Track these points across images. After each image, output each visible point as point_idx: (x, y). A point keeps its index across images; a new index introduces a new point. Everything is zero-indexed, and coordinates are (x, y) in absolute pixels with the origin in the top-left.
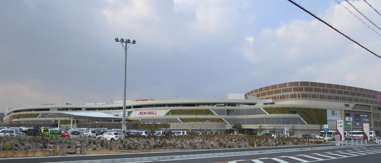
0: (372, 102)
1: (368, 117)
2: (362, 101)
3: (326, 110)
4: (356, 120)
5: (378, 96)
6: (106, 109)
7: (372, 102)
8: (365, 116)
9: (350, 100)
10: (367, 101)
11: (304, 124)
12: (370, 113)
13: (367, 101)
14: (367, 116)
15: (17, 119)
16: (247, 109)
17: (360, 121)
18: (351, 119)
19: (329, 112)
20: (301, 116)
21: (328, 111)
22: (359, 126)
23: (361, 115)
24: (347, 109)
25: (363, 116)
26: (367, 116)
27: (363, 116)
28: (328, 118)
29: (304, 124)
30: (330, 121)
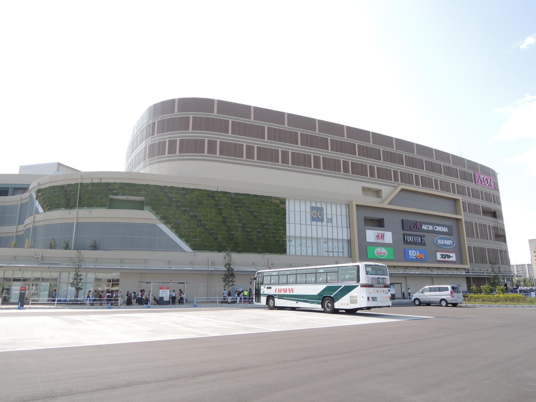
0: (461, 190)
1: (449, 234)
2: (427, 182)
3: (283, 202)
4: (405, 242)
5: (481, 176)
6: (367, 286)
7: (461, 190)
8: (439, 229)
9: (384, 175)
10: (445, 186)
11: (176, 248)
12: (458, 220)
13: (445, 186)
14: (445, 230)
15: (439, 292)
16: (78, 224)
17: (422, 243)
18: (388, 237)
19: (298, 214)
20: (166, 220)
21: (291, 207)
22: (417, 260)
23: (424, 227)
24: (371, 201)
25: (431, 228)
26: (445, 230)
27: (431, 228)
28: (291, 230)
29: (176, 248)
30: (304, 241)
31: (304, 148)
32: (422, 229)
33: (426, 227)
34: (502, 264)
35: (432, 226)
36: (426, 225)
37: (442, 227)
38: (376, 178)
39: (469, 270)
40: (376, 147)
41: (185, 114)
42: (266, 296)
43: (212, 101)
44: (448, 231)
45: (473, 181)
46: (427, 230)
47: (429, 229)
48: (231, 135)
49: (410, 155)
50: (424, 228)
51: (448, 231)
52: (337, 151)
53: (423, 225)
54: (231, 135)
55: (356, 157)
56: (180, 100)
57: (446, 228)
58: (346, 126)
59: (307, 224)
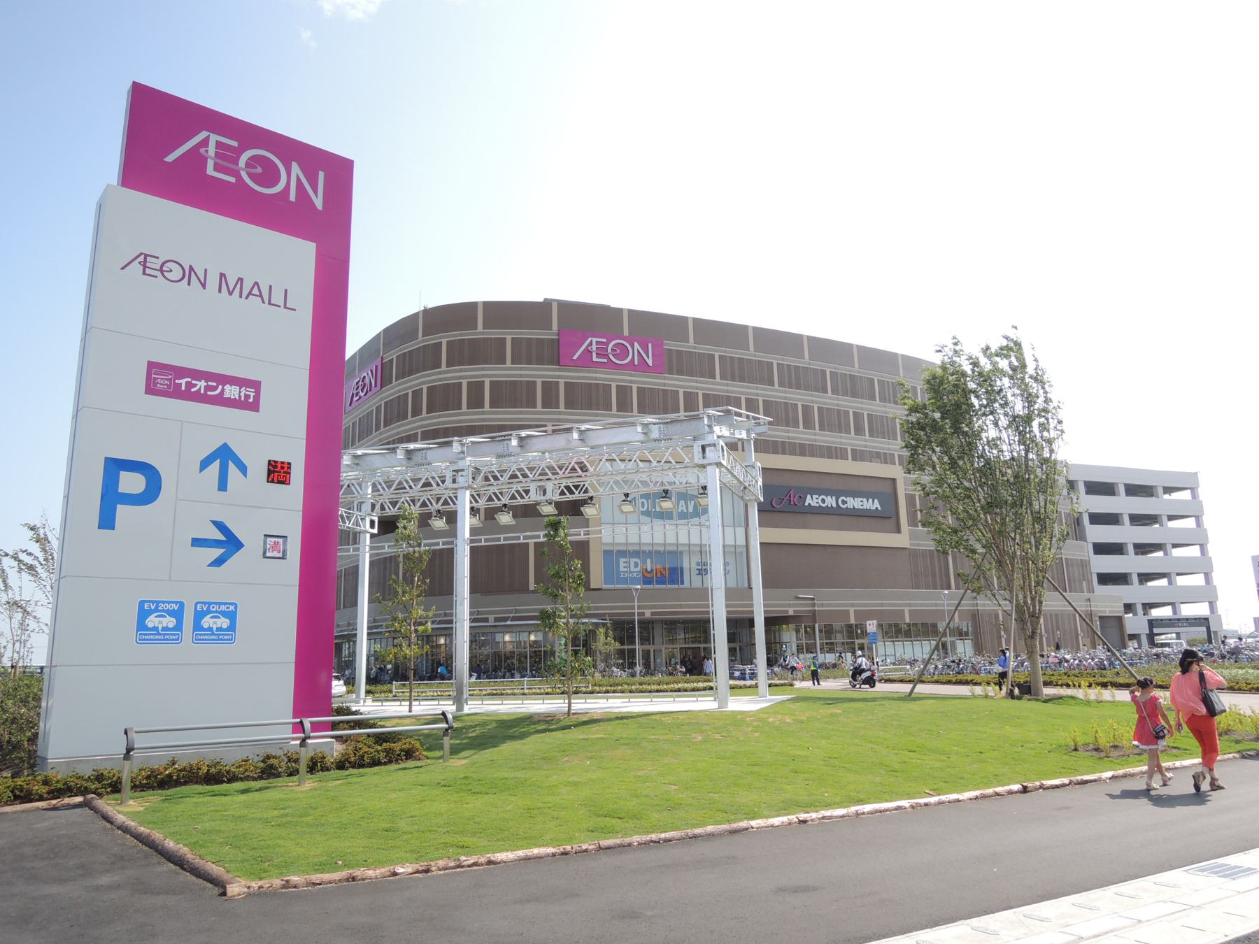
25: (830, 501)
27: (830, 501)
31: (697, 380)
32: (806, 504)
33: (817, 501)
34: (1070, 592)
35: (834, 498)
36: (817, 496)
37: (865, 500)
38: (867, 437)
39: (977, 606)
40: (764, 357)
41: (432, 340)
42: (573, 710)
43: (473, 306)
44: (879, 508)
45: (875, 397)
46: (820, 506)
47: (823, 505)
48: (798, 403)
49: (793, 362)
50: (811, 502)
51: (879, 508)
52: (733, 380)
53: (809, 496)
54: (680, 389)
55: (716, 382)
56: (486, 304)
57: (876, 501)
58: (693, 318)
59: (611, 522)
